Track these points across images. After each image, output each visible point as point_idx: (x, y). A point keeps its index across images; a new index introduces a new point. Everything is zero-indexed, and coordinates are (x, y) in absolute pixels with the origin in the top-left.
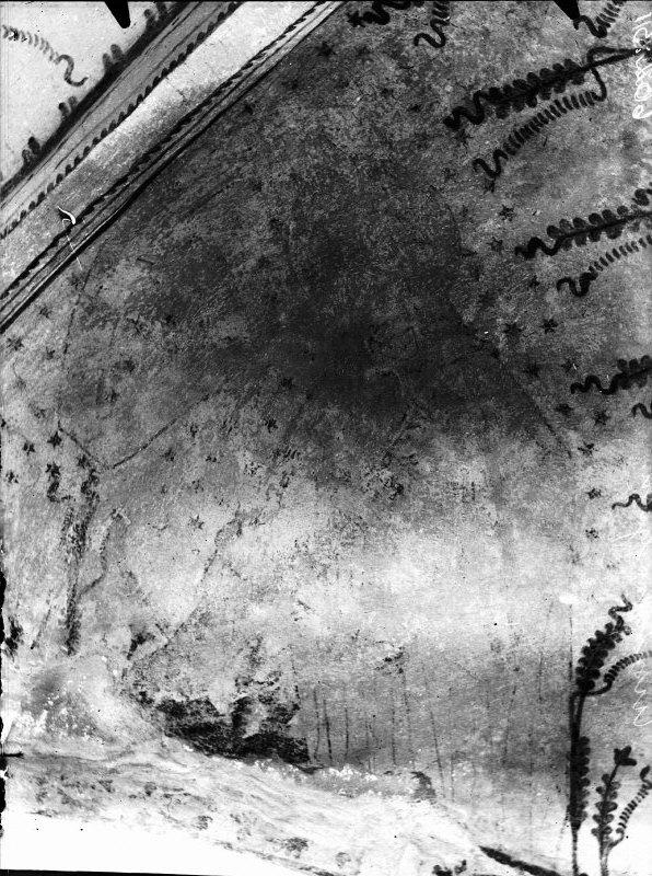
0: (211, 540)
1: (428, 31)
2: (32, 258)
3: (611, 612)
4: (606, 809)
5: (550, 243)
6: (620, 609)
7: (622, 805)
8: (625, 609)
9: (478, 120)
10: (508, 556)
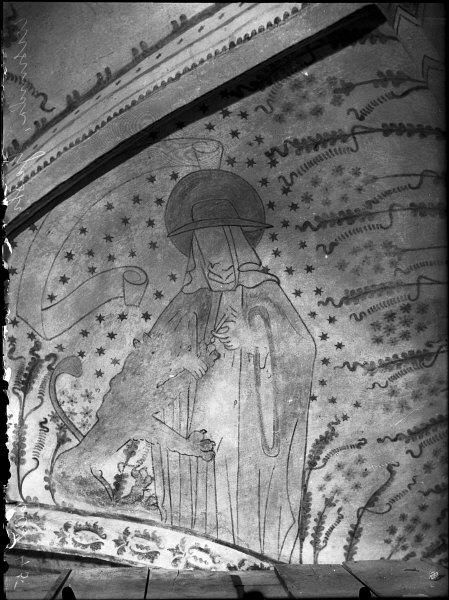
0: (107, 383)
1: (265, 105)
2: (411, 172)
3: (329, 425)
4: (318, 529)
5: (315, 224)
6: (333, 423)
7: (327, 527)
8: (336, 424)
9: (285, 155)
10: (434, 282)
